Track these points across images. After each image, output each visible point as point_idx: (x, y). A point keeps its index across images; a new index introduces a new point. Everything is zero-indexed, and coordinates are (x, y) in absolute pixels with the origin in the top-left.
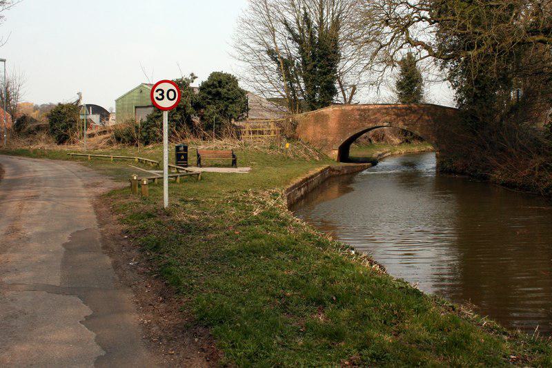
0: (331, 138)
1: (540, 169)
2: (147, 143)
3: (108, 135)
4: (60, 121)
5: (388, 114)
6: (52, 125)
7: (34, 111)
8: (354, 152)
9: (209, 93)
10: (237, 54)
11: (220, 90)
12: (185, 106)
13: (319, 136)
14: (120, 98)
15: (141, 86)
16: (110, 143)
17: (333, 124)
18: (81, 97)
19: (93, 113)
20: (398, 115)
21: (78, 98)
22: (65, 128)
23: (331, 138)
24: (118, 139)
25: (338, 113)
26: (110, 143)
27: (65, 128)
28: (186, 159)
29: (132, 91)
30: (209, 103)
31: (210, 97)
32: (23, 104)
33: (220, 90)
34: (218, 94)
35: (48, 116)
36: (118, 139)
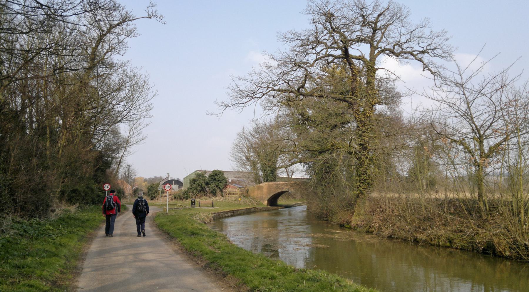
0: (264, 196)
1: (454, 205)
2: (187, 199)
3: (172, 196)
4: (152, 191)
5: (287, 186)
6: (149, 192)
7: (144, 182)
8: (281, 201)
9: (212, 178)
10: (233, 159)
11: (216, 177)
12: (202, 184)
13: (259, 195)
14: (186, 178)
15: (196, 171)
16: (172, 199)
17: (265, 190)
18: (169, 176)
19: (175, 184)
20: (291, 186)
21: (167, 176)
22: (154, 193)
23: (264, 196)
24: (175, 198)
25: (267, 185)
26: (172, 199)
27: (154, 193)
28: (194, 204)
29: (191, 174)
30: (212, 183)
31: (212, 180)
32: (138, 178)
33: (216, 177)
34: (215, 179)
35: (147, 188)
36: (175, 198)
